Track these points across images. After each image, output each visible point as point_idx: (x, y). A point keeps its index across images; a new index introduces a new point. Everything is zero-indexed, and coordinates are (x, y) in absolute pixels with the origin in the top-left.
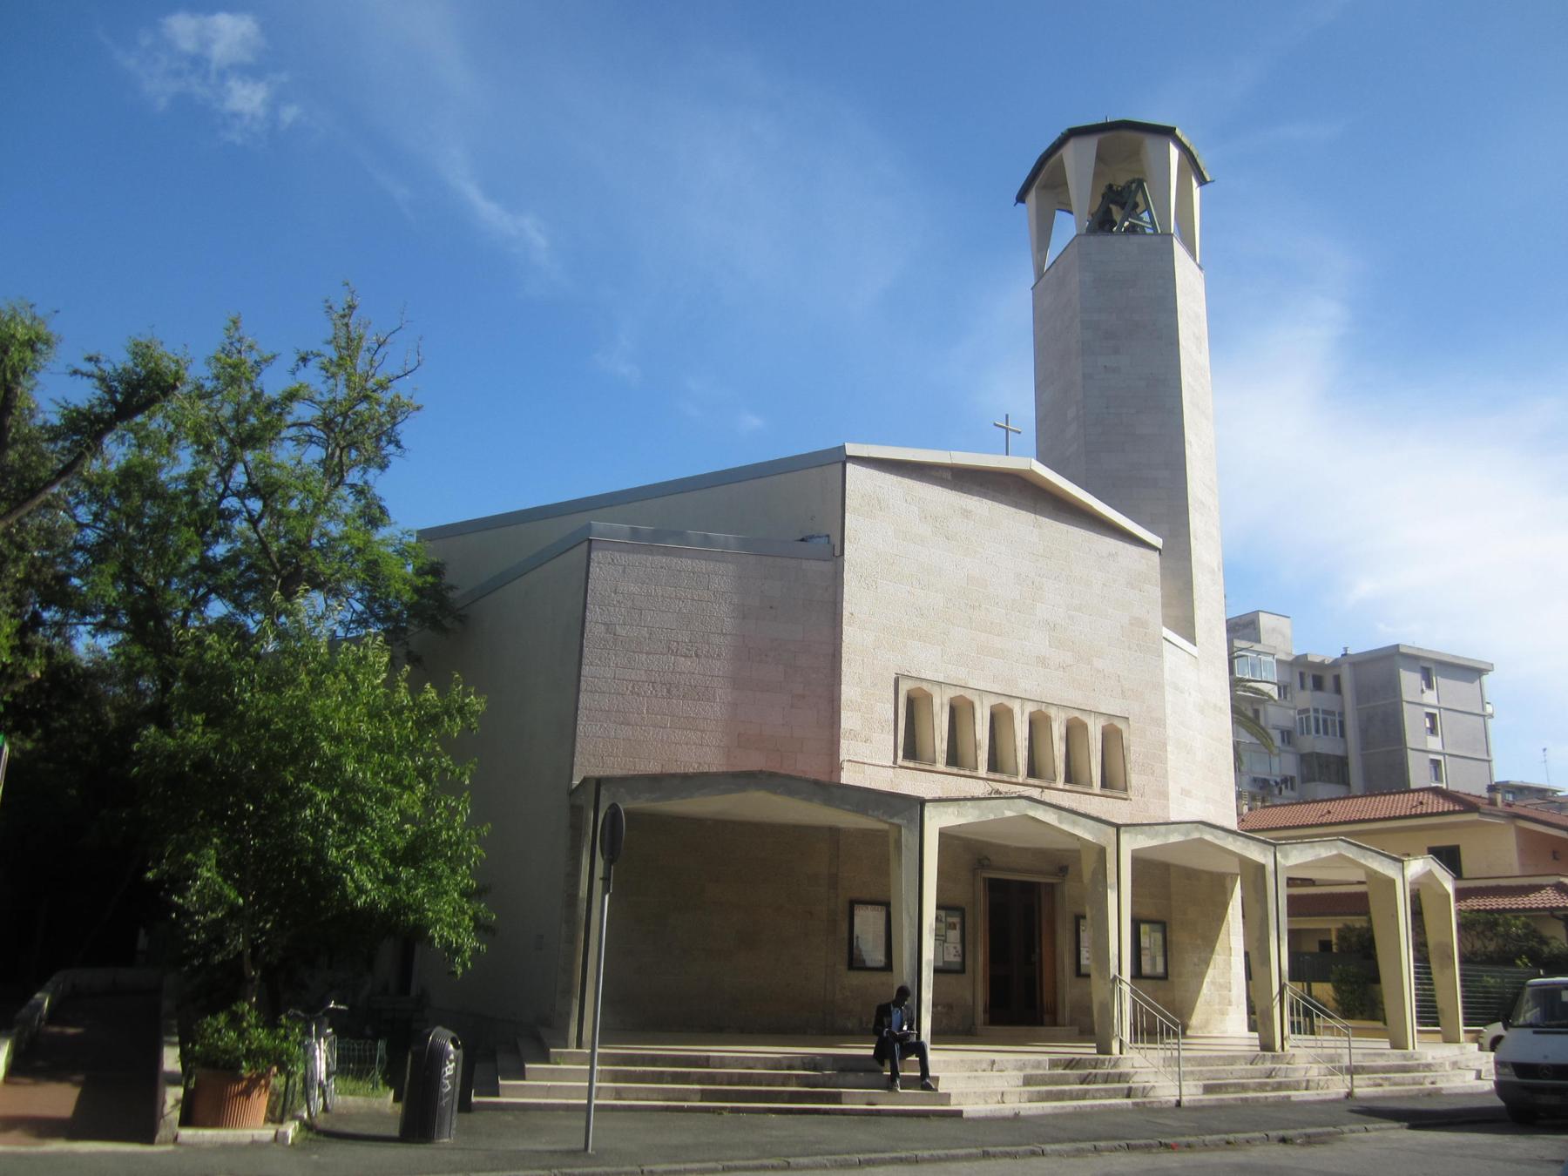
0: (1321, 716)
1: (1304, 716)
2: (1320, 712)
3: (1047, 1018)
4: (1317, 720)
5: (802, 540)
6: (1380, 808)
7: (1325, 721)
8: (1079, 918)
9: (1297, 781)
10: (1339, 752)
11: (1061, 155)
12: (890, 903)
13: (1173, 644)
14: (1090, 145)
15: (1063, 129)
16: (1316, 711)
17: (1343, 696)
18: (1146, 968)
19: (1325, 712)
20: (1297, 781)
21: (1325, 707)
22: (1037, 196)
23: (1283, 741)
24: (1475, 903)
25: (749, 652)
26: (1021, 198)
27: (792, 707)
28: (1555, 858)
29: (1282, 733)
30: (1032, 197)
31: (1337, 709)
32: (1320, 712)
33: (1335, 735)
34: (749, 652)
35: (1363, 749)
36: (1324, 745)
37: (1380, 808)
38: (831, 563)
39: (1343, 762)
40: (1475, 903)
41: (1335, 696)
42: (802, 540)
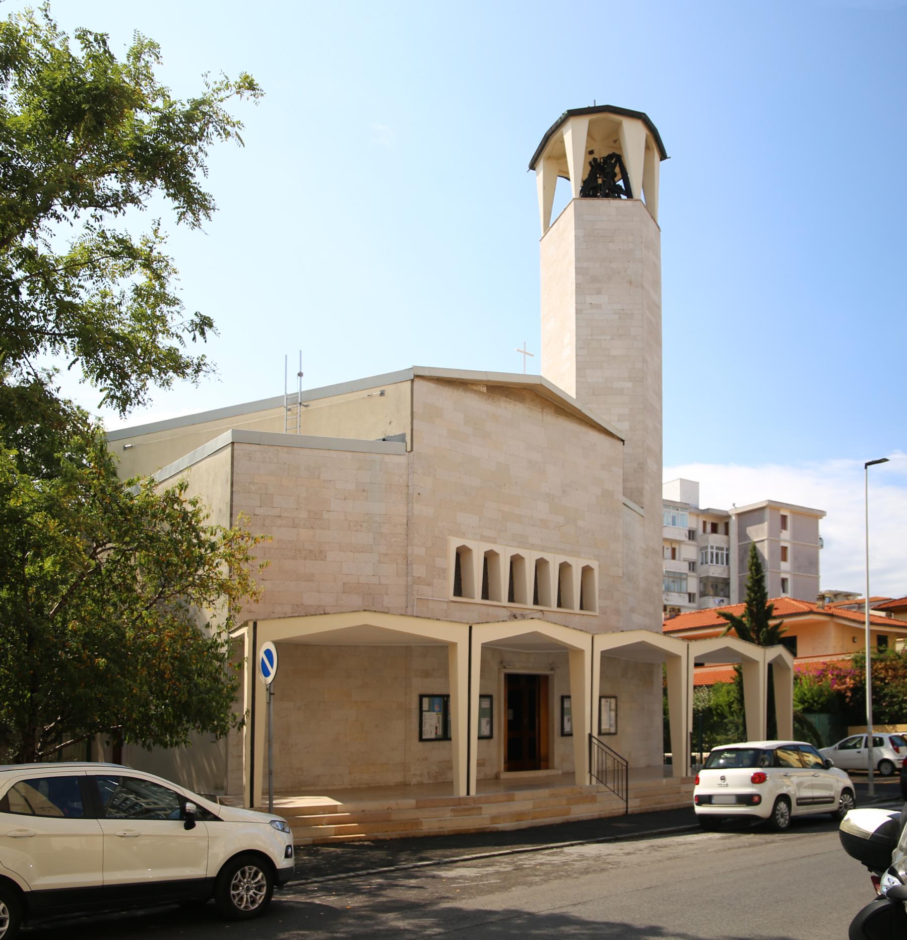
0: (715, 551)
1: (704, 551)
2: (715, 548)
3: (542, 763)
4: (712, 554)
5: (384, 440)
6: (620, 788)
7: (717, 555)
8: (565, 698)
9: (697, 596)
10: (725, 576)
11: (562, 132)
12: (448, 696)
13: (559, 218)
14: (583, 123)
15: (564, 111)
16: (712, 548)
17: (729, 537)
18: (604, 727)
19: (717, 548)
20: (697, 596)
21: (718, 545)
22: (544, 166)
23: (690, 569)
24: (297, 840)
25: (349, 524)
26: (533, 166)
27: (379, 562)
28: (854, 642)
29: (690, 563)
30: (541, 165)
31: (724, 546)
32: (715, 548)
33: (723, 564)
34: (349, 524)
35: (739, 573)
36: (716, 571)
37: (620, 788)
38: (405, 457)
39: (726, 582)
40: (297, 840)
41: (725, 537)
42: (384, 440)
